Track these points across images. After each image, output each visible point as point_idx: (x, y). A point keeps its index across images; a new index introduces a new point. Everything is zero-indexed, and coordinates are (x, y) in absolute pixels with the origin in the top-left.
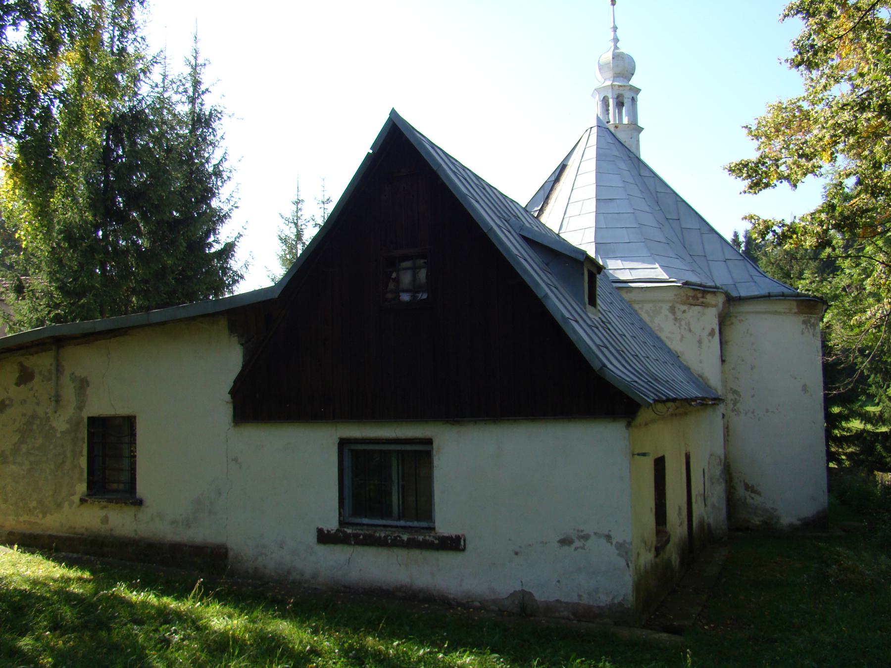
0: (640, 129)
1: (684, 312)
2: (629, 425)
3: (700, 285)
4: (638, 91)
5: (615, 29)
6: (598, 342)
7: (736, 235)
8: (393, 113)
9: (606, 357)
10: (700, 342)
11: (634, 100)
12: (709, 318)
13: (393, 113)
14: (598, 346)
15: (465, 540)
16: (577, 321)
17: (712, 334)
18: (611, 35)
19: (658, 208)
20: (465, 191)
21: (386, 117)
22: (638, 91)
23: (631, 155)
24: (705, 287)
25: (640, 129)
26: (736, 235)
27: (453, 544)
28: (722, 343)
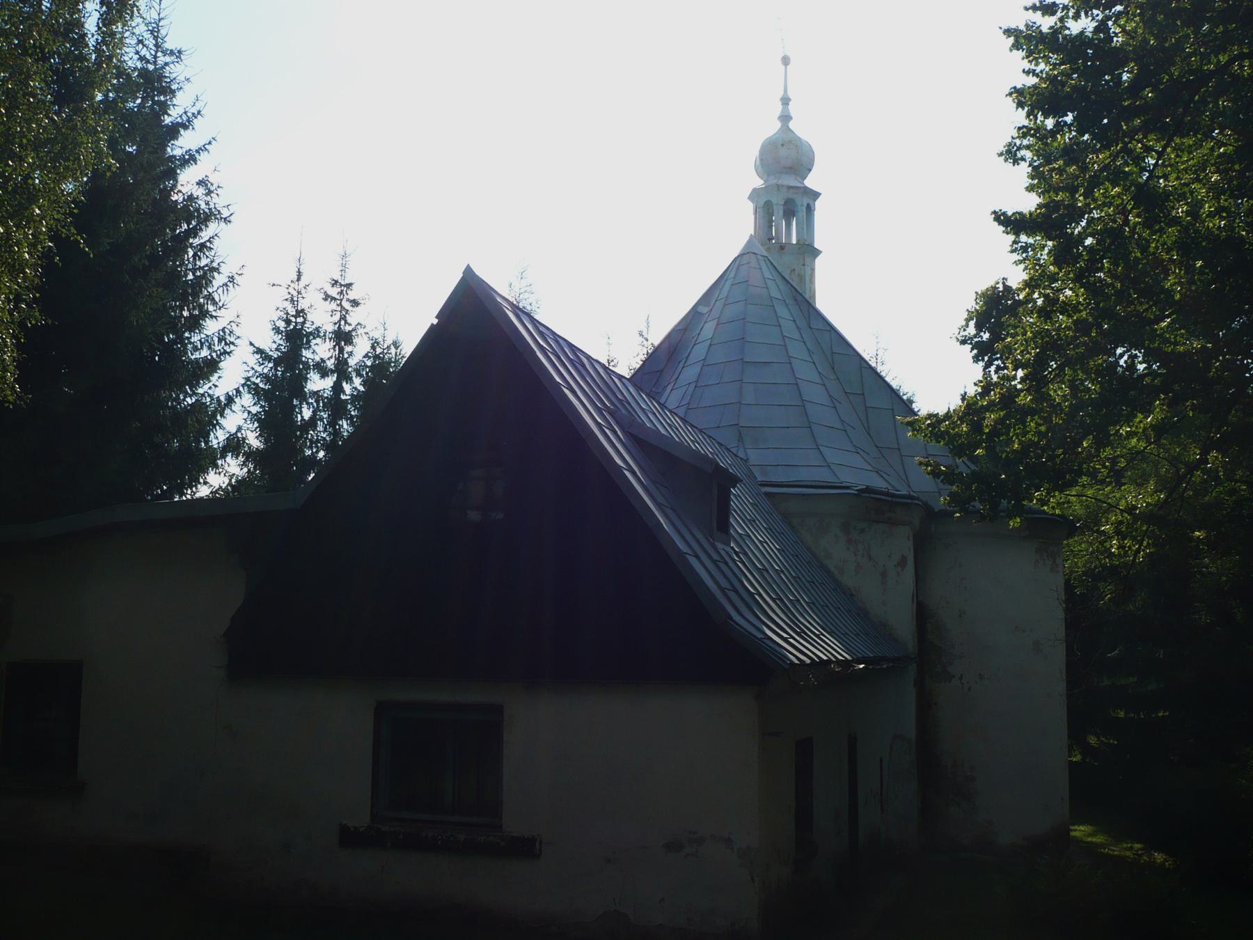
0: (816, 253)
1: (862, 531)
2: (206, 218)
3: (887, 494)
4: (816, 195)
5: (786, 101)
6: (724, 584)
7: (1017, 263)
8: (468, 272)
9: (698, 541)
10: (884, 575)
11: (810, 210)
12: (902, 542)
13: (468, 272)
14: (723, 590)
15: (541, 843)
16: (697, 557)
17: (902, 562)
18: (778, 108)
19: (833, 377)
20: (558, 380)
21: (458, 276)
22: (816, 195)
23: (799, 298)
24: (893, 496)
25: (816, 253)
26: (1017, 263)
27: (526, 848)
28: (919, 579)
